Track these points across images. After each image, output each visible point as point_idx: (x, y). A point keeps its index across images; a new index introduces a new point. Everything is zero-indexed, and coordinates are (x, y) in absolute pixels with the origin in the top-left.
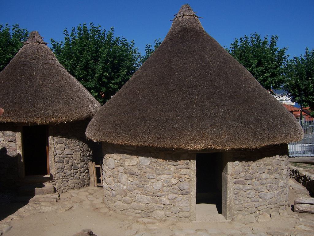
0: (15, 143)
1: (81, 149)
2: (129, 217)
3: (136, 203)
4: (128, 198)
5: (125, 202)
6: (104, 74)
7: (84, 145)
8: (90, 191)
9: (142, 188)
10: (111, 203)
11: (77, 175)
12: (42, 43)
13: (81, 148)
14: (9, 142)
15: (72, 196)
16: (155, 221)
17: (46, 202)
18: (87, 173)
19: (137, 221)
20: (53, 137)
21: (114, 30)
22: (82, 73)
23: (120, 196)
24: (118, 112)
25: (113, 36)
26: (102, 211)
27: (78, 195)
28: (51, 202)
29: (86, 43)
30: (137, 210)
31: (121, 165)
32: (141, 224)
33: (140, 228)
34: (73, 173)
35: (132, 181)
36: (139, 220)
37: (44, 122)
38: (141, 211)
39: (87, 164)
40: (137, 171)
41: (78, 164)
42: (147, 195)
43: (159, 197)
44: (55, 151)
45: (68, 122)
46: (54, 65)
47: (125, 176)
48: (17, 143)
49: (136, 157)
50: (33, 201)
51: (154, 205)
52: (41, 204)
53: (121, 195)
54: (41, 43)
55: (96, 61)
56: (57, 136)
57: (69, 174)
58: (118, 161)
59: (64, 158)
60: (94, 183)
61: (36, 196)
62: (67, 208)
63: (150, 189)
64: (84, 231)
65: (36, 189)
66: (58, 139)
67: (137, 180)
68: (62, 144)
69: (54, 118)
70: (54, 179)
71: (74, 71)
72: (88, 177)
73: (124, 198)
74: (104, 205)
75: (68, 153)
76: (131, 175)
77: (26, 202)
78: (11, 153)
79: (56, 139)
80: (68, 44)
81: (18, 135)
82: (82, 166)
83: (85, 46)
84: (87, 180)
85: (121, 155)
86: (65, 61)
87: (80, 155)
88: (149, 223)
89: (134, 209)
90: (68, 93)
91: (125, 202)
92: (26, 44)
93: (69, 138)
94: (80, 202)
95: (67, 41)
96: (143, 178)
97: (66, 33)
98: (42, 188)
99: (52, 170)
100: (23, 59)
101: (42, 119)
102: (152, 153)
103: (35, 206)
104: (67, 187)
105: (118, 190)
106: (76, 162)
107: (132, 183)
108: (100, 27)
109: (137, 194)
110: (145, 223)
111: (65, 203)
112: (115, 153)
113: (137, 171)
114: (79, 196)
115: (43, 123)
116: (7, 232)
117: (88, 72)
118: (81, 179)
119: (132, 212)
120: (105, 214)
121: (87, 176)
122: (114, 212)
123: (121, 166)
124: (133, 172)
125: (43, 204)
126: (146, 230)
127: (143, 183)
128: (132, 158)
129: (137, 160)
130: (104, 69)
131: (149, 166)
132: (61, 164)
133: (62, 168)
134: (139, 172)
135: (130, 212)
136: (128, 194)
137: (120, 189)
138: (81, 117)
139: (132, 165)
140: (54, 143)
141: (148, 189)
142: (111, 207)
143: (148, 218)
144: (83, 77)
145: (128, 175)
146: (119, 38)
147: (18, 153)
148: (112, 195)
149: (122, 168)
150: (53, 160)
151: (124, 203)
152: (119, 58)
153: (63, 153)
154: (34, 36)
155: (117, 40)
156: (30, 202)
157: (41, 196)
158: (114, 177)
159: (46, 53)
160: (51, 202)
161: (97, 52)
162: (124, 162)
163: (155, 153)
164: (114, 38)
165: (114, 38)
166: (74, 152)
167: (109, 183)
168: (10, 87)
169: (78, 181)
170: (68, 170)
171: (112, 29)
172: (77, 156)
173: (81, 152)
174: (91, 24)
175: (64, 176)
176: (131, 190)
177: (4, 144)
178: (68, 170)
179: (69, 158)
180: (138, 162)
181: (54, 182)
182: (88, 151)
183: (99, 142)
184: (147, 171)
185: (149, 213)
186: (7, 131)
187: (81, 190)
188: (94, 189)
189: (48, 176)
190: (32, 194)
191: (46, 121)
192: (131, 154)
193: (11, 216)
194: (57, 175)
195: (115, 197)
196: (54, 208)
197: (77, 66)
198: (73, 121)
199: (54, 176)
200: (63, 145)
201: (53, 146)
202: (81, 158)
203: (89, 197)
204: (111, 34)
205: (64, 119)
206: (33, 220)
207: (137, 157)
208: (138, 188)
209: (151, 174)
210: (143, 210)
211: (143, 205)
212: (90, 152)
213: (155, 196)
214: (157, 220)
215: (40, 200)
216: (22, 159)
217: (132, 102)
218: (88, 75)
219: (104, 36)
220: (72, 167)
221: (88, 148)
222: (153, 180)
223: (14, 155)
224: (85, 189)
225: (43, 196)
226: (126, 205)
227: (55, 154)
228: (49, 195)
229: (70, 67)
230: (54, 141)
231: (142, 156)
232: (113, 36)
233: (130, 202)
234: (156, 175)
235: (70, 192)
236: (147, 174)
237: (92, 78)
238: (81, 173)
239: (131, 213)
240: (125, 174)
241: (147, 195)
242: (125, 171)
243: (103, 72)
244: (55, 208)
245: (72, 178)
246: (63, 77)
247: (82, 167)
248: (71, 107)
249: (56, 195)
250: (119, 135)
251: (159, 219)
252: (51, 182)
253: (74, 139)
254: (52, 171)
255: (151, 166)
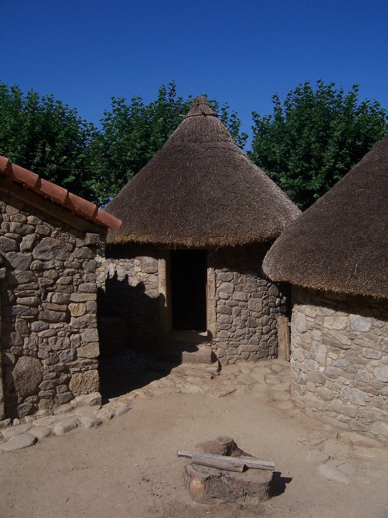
0: (156, 277)
1: (263, 293)
2: (326, 426)
3: (340, 402)
4: (326, 389)
5: (321, 396)
6: (337, 166)
7: (270, 286)
8: (274, 367)
9: (353, 375)
10: (298, 394)
11: (255, 337)
12: (209, 115)
13: (264, 292)
14: (148, 275)
15: (240, 371)
16: (373, 442)
17: (195, 377)
18: (274, 336)
19: (338, 437)
20: (215, 270)
21: (358, 88)
22: (301, 166)
23: (314, 384)
24: (315, 228)
25: (356, 100)
26: (282, 406)
27: (251, 372)
28: (203, 377)
29: (309, 114)
30: (342, 415)
31: (317, 326)
32: (342, 444)
33: (339, 451)
34: (247, 332)
35: (335, 358)
36: (342, 434)
37: (197, 244)
38: (349, 418)
39: (275, 319)
40: (344, 342)
41: (256, 318)
42: (362, 388)
43: (385, 397)
44: (217, 293)
45: (238, 246)
46: (225, 148)
47: (323, 348)
48: (159, 276)
49: (344, 314)
50: (177, 372)
51: (374, 410)
52: (187, 379)
53: (314, 383)
54: (208, 115)
55: (325, 143)
56: (221, 268)
57: (239, 334)
58: (312, 320)
59: (232, 306)
60: (285, 354)
61: (184, 365)
62: (225, 393)
63: (368, 378)
64: (221, 439)
65: (184, 353)
66: (223, 273)
67: (343, 358)
68: (229, 281)
69: (213, 237)
70: (214, 340)
71: (287, 162)
72: (276, 341)
73: (319, 388)
74: (288, 397)
75: (240, 298)
76: (333, 348)
77: (165, 373)
78: (150, 292)
79: (220, 273)
80: (279, 118)
81: (161, 264)
82: (265, 321)
83: (307, 119)
84: (273, 348)
85: (318, 308)
86: (273, 146)
87: (261, 303)
88: (360, 444)
89: (335, 411)
90: (241, 195)
91: (321, 396)
92: (185, 118)
93: (242, 272)
94: (250, 385)
95: (277, 113)
96: (356, 355)
97: (275, 101)
98: (192, 353)
99: (211, 326)
100: (178, 142)
101: (194, 238)
102: (374, 310)
103: (177, 380)
104: (235, 356)
105: (309, 373)
106: (253, 314)
107: (335, 363)
108: (333, 85)
109: (343, 384)
110: (352, 444)
111: (226, 383)
112: (308, 304)
113: (345, 340)
114: (253, 373)
115: (195, 245)
116: (120, 414)
117: (310, 163)
118: (261, 345)
119: (332, 417)
120: (284, 412)
121: (274, 340)
122: (302, 411)
123: (318, 329)
124: (337, 342)
125: (189, 379)
126: (350, 457)
127: (355, 364)
128: (338, 316)
129: (346, 321)
130: (337, 157)
131: (368, 333)
132: (227, 316)
133: (228, 323)
134: (349, 343)
135: (328, 416)
136: (327, 382)
137: (314, 371)
138: (261, 238)
139: (335, 328)
140: (216, 280)
141: (365, 377)
142: (297, 401)
143: (361, 434)
144: (301, 173)
145: (329, 347)
146: (369, 101)
147: (160, 292)
148: (300, 379)
149: (319, 333)
150: (213, 308)
151: (319, 397)
152: (366, 138)
153: (231, 298)
154: (198, 105)
155: (364, 107)
156: (171, 373)
157: (191, 365)
158: (304, 348)
159: (214, 130)
160: (203, 377)
161: (327, 128)
162: (322, 322)
163: (381, 310)
164: (358, 103)
165: (358, 103)
166: (250, 296)
167: (297, 358)
168: (153, 187)
169: (256, 347)
170: (238, 327)
171: (354, 87)
172: (256, 304)
173: (263, 297)
174: (318, 82)
175: (231, 336)
176: (331, 376)
177: (141, 276)
178: (238, 327)
179: (241, 306)
180: (348, 324)
181: (214, 344)
182: (278, 297)
183: (278, 282)
184: (363, 344)
185: (364, 425)
186: (146, 257)
187: (261, 363)
188: (283, 364)
189: (205, 334)
190: (178, 361)
191: (200, 243)
192: (336, 309)
193: (136, 392)
194: (219, 334)
195: (304, 384)
196: (204, 389)
197: (291, 154)
198: (247, 244)
199: (214, 335)
200: (231, 285)
201: (213, 284)
202: (264, 308)
203: (269, 378)
204: (353, 96)
205: (231, 240)
206: (164, 403)
207: (347, 314)
208: (345, 373)
209: (371, 350)
210: (353, 415)
211: (352, 406)
212: (281, 298)
213: (377, 394)
214: (380, 441)
215: (187, 373)
216: (166, 303)
217: (343, 210)
218: (310, 169)
219: (340, 100)
220: (246, 323)
221: (278, 292)
222: (374, 362)
223: (155, 295)
224: (267, 363)
225: (194, 366)
226: (322, 402)
227: (217, 298)
228: (203, 365)
229: (281, 156)
230: (216, 277)
231: (355, 313)
232: (356, 100)
233: (329, 397)
234: (380, 353)
235: (240, 364)
236: (364, 349)
237: (317, 174)
238: (262, 334)
239: (332, 419)
240: (323, 345)
241: (362, 388)
242: (324, 339)
243: (335, 163)
244: (206, 389)
245: (245, 341)
246: (238, 169)
247: (264, 324)
248: (244, 219)
249: (214, 367)
250: (310, 272)
251: (383, 440)
252: (209, 344)
253: (252, 275)
254: (211, 326)
255: (372, 334)
